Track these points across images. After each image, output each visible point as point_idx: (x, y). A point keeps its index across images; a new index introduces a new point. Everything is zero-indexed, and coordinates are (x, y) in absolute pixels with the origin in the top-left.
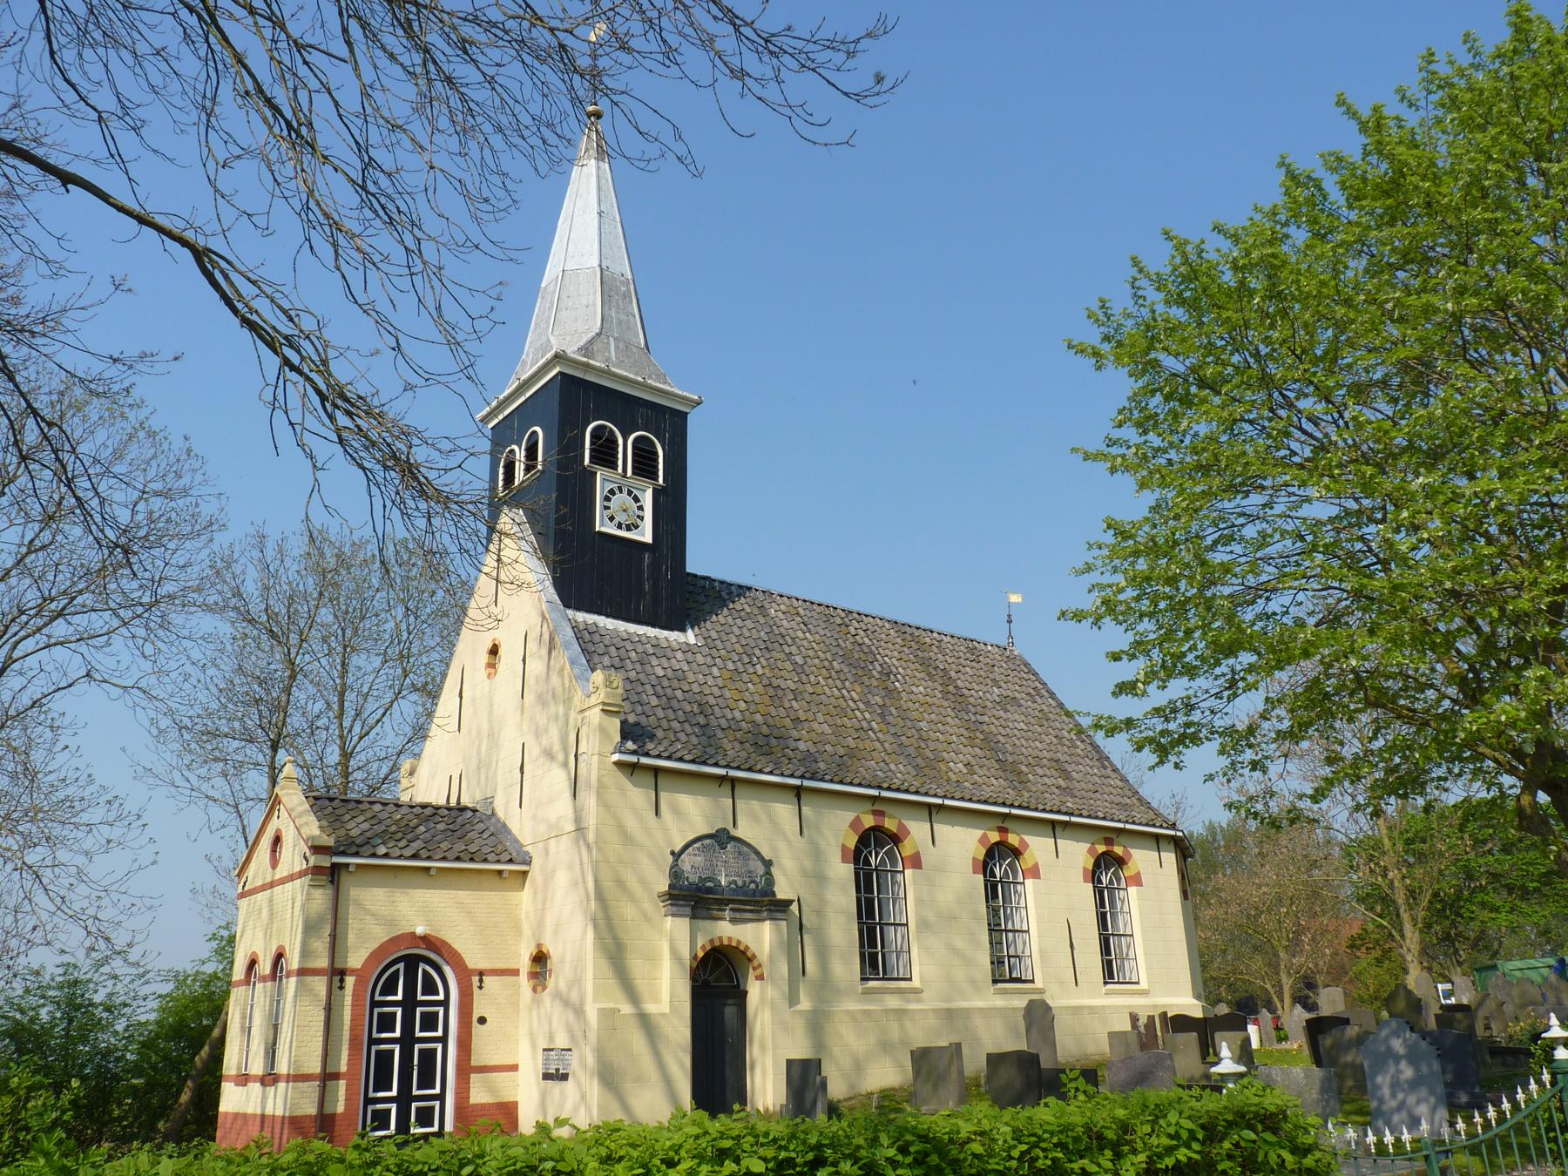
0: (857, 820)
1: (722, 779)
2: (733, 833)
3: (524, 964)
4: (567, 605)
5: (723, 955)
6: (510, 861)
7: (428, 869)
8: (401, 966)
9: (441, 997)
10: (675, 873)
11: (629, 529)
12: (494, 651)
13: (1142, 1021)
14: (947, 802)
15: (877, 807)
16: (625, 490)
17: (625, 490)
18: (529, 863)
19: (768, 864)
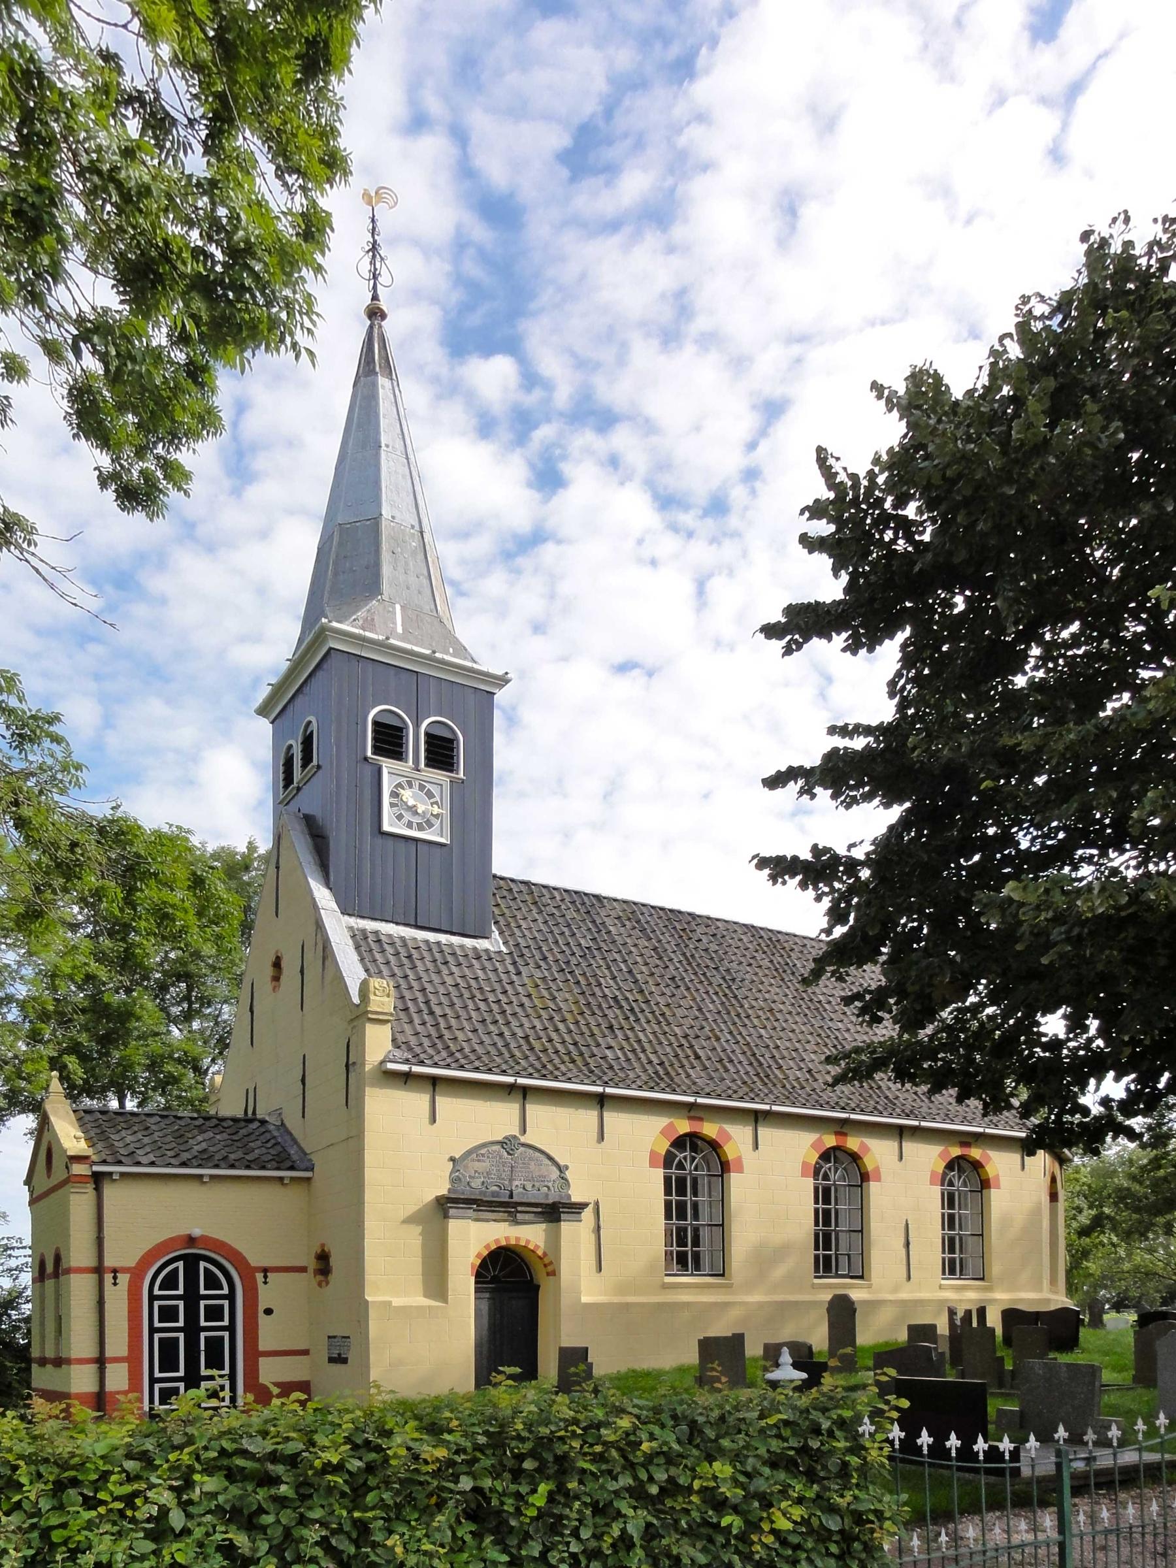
0: (819, 1140)
1: (511, 1089)
2: (523, 1139)
3: (312, 1264)
4: (344, 912)
5: (513, 1252)
6: (292, 1168)
7: (201, 1176)
8: (180, 1264)
9: (226, 1291)
11: (420, 827)
12: (277, 964)
13: (960, 1314)
14: (700, 1100)
15: (692, 1114)
16: (416, 784)
17: (416, 784)
18: (312, 1170)
19: (562, 1169)
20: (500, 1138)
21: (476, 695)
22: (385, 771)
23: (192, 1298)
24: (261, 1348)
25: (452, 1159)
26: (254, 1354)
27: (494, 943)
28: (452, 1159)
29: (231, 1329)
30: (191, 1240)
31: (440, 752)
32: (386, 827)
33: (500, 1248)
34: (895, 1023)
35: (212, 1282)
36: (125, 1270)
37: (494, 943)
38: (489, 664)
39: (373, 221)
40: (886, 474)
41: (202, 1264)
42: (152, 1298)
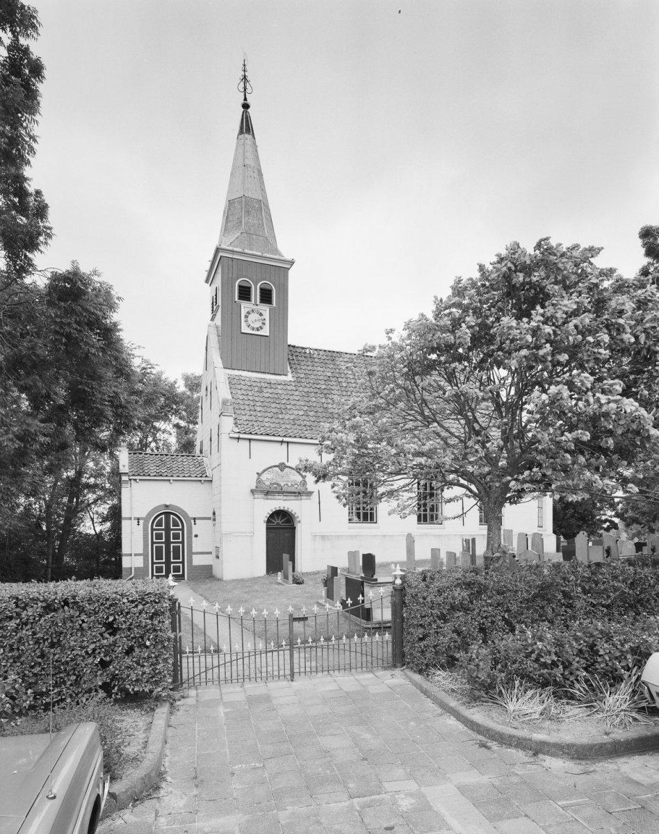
2: (287, 464)
8: (163, 516)
9: (180, 527)
10: (259, 481)
11: (258, 330)
20: (278, 464)
21: (281, 270)
22: (242, 307)
23: (168, 530)
24: (193, 551)
25: (258, 474)
26: (191, 553)
27: (289, 377)
28: (258, 474)
29: (183, 542)
30: (167, 506)
31: (266, 296)
32: (243, 331)
33: (280, 510)
34: (9, 531)
35: (176, 524)
36: (142, 518)
37: (289, 377)
38: (287, 256)
39: (244, 65)
40: (157, 424)
41: (172, 516)
42: (153, 530)
